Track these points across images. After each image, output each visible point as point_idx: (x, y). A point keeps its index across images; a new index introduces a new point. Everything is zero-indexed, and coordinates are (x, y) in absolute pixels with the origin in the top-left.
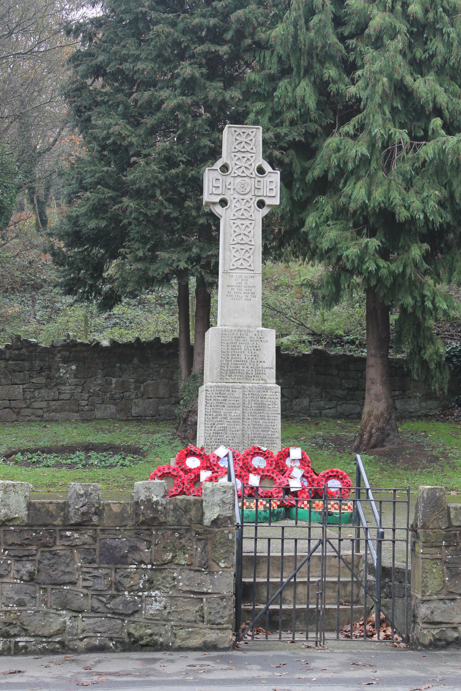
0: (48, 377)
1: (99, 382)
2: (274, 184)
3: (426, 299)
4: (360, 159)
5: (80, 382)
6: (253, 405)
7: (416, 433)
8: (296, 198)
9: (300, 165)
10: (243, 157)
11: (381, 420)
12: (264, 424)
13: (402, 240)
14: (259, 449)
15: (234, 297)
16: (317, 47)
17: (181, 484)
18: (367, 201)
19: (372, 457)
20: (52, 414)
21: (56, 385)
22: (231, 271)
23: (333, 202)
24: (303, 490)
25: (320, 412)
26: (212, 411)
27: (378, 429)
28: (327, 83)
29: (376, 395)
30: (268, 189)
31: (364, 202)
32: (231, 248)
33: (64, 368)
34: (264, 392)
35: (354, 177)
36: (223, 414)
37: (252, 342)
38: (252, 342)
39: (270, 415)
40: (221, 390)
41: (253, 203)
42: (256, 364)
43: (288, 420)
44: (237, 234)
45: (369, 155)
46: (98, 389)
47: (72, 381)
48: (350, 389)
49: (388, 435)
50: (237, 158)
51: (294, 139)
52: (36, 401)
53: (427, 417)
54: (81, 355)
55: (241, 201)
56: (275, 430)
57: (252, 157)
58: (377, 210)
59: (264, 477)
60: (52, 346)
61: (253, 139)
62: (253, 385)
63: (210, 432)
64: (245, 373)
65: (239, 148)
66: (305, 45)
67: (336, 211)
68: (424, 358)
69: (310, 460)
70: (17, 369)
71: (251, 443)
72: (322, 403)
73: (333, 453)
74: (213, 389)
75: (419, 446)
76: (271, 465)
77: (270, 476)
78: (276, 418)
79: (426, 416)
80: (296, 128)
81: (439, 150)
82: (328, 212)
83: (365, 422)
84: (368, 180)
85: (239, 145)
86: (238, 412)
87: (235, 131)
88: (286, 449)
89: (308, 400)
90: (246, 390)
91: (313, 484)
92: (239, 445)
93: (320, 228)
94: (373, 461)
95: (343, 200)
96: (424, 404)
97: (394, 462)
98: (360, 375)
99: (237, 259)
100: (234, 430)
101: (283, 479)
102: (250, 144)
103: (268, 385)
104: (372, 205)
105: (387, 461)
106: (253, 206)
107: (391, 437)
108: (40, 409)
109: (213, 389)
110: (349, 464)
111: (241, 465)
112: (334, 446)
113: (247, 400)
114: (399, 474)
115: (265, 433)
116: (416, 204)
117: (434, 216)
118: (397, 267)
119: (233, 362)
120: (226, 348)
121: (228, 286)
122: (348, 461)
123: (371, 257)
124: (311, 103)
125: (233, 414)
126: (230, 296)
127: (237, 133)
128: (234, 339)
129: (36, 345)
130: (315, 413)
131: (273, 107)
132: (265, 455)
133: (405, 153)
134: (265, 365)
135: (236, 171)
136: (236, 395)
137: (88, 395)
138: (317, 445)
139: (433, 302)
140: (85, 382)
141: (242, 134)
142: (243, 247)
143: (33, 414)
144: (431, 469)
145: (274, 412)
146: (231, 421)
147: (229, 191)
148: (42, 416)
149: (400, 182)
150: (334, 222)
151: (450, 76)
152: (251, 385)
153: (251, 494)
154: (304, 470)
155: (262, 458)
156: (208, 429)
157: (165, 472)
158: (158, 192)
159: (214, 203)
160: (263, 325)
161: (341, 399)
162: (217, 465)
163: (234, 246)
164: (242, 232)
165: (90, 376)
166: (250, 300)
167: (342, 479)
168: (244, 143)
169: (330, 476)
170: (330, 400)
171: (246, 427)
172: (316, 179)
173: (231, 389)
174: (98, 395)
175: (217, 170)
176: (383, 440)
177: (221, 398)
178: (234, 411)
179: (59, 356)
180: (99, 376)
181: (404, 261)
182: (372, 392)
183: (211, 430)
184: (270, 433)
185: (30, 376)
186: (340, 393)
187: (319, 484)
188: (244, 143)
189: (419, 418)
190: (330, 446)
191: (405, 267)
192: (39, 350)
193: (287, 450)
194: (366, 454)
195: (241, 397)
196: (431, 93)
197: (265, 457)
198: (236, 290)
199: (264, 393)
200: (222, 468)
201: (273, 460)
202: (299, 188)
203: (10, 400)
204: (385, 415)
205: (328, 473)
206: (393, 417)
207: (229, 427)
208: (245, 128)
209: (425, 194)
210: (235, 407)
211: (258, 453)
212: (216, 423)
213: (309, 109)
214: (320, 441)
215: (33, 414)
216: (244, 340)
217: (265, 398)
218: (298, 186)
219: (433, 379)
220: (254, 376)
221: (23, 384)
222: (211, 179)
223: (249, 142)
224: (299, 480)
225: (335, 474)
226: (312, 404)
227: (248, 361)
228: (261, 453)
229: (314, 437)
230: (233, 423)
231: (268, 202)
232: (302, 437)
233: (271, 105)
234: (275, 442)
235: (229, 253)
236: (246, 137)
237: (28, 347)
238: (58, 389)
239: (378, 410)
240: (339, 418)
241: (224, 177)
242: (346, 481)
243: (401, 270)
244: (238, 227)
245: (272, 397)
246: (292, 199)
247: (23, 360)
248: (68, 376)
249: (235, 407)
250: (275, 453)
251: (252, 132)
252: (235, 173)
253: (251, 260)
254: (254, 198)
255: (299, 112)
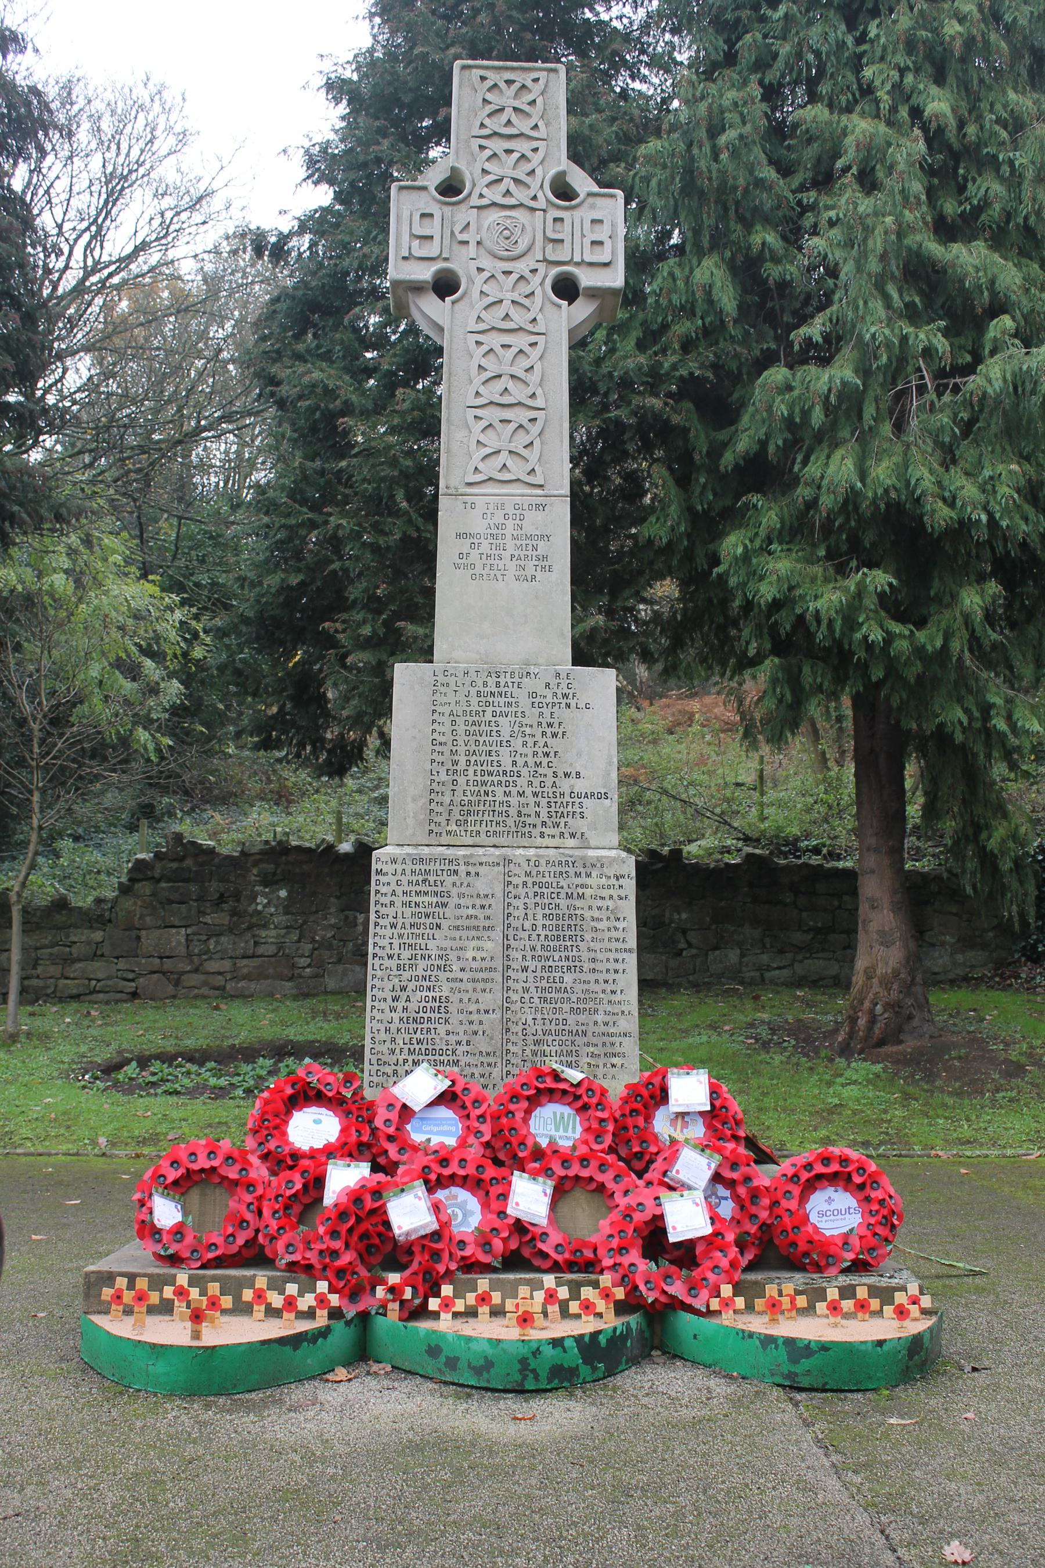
0: (234, 913)
1: (333, 921)
2: (606, 227)
3: (993, 712)
4: (840, 396)
5: (296, 921)
6: (540, 923)
7: (958, 1013)
8: (699, 508)
9: (707, 437)
10: (509, 152)
11: (895, 986)
12: (578, 987)
13: (936, 584)
14: (556, 1076)
15: (478, 570)
16: (735, 188)
17: (249, 1216)
18: (859, 485)
19: (878, 1068)
20: (242, 984)
21: (250, 927)
22: (469, 490)
23: (781, 509)
24: (712, 1241)
25: (762, 975)
26: (396, 942)
27: (887, 1006)
28: (760, 258)
29: (882, 933)
30: (587, 242)
31: (852, 488)
32: (471, 420)
33: (265, 895)
34: (578, 875)
35: (825, 445)
36: (434, 953)
37: (536, 711)
38: (536, 711)
39: (599, 956)
40: (427, 872)
41: (542, 284)
42: (549, 781)
43: (698, 992)
44: (488, 374)
45: (859, 382)
46: (329, 935)
47: (280, 919)
48: (817, 931)
49: (910, 1017)
50: (488, 153)
51: (691, 374)
52: (210, 959)
53: (965, 980)
54: (298, 870)
55: (501, 277)
56: (617, 1009)
57: (535, 150)
58: (883, 506)
59: (567, 1185)
60: (243, 853)
61: (539, 101)
62: (541, 851)
63: (388, 1015)
64: (513, 812)
65: (495, 124)
66: (710, 179)
67: (787, 527)
68: (989, 848)
69: (740, 1116)
70: (176, 896)
71: (534, 1053)
72: (765, 958)
73: (794, 1060)
74: (399, 867)
75: (974, 1041)
76: (598, 1135)
77: (591, 1179)
78: (619, 966)
79: (966, 979)
80: (694, 354)
81: (1014, 375)
82: (771, 523)
83: (861, 991)
84: (857, 447)
85: (495, 119)
86: (489, 945)
87: (483, 79)
88: (656, 1074)
89: (738, 952)
90: (516, 870)
91: (754, 1210)
92: (491, 1060)
93: (754, 561)
94: (883, 1076)
95: (803, 492)
96: (960, 958)
97: (930, 1077)
98: (836, 903)
99: (488, 451)
100: (473, 1007)
101: (642, 1194)
102: (528, 115)
103: (591, 853)
104: (870, 495)
105: (912, 1075)
106: (538, 292)
107: (915, 1022)
108: (220, 973)
109: (399, 867)
110: (830, 1084)
111: (487, 1137)
112: (793, 1042)
113: (519, 903)
114: (944, 1105)
115: (582, 1018)
116: (969, 491)
117: (1011, 519)
118: (930, 638)
119: (471, 777)
120: (447, 728)
121: (459, 536)
122: (827, 1077)
123: (871, 615)
124: (728, 300)
125: (470, 954)
126: (465, 566)
127: (489, 83)
128: (474, 700)
129: (211, 852)
130: (752, 978)
131: (646, 321)
132: (578, 1097)
133: (934, 396)
134: (580, 786)
135: (485, 191)
136: (481, 886)
137: (310, 946)
138: (757, 1040)
139: (1009, 718)
140: (305, 922)
141: (502, 85)
142: (507, 414)
143: (205, 983)
144: (1014, 1094)
145: (614, 945)
146: (464, 976)
147: (463, 248)
148: (223, 988)
149: (930, 450)
150: (785, 547)
151: (1019, 248)
152: (532, 852)
153: (516, 1253)
154: (718, 1158)
155: (567, 1111)
156: (383, 1005)
157: (196, 1167)
158: (400, 495)
159: (417, 288)
160: (576, 662)
161: (800, 949)
162: (399, 1138)
163: (479, 412)
164: (507, 369)
165: (314, 909)
166: (533, 578)
167: (861, 1187)
168: (509, 111)
169: (819, 1177)
170: (781, 952)
171: (515, 997)
172: (742, 462)
173: (462, 869)
174: (330, 947)
175: (424, 188)
176: (900, 1030)
177: (427, 899)
178: (475, 943)
179: (255, 871)
180: (333, 910)
181: (943, 625)
182: (873, 926)
183: (393, 1010)
184: (600, 1018)
185: (199, 912)
186: (798, 937)
187: (777, 1211)
188: (509, 111)
189: (952, 982)
190: (785, 1044)
191: (947, 636)
192: (216, 860)
193: (657, 1081)
194: (865, 1060)
195: (499, 895)
196: (985, 270)
197: (580, 1104)
198: (485, 547)
199: (578, 881)
200: (415, 1148)
201: (605, 1115)
202: (704, 486)
203: (161, 958)
204: (902, 976)
205: (808, 1166)
206: (919, 978)
207: (454, 998)
208: (513, 69)
209: (987, 473)
210: (476, 928)
211: (551, 1091)
212: (411, 985)
213: (721, 311)
214: (764, 1032)
215: (205, 983)
216: (510, 704)
217: (581, 897)
218: (702, 480)
219: (1003, 895)
220: (544, 824)
221: (186, 927)
222: (406, 214)
223: (527, 108)
224: (699, 1195)
225: (835, 1167)
226: (745, 959)
227: (524, 772)
228: (564, 1092)
229: (751, 1025)
230: (470, 986)
231: (586, 279)
232: (725, 1024)
233: (641, 316)
234: (617, 1049)
235: (465, 432)
236: (517, 95)
237: (196, 855)
238: (254, 936)
239: (887, 964)
240: (799, 986)
241: (447, 210)
242: (878, 1194)
243: (939, 644)
244: (491, 356)
245: (605, 893)
246: (690, 509)
247: (187, 881)
248: (273, 910)
249: (476, 928)
250: (616, 1088)
251: (536, 80)
252: (481, 196)
253: (533, 455)
254: (542, 268)
255: (700, 322)
